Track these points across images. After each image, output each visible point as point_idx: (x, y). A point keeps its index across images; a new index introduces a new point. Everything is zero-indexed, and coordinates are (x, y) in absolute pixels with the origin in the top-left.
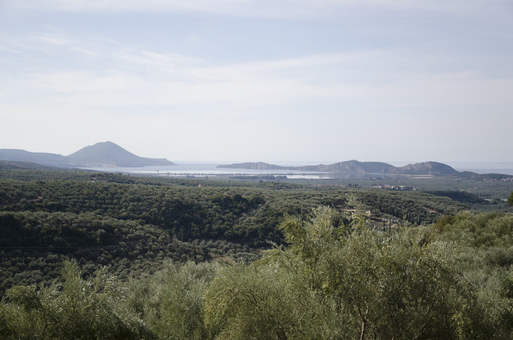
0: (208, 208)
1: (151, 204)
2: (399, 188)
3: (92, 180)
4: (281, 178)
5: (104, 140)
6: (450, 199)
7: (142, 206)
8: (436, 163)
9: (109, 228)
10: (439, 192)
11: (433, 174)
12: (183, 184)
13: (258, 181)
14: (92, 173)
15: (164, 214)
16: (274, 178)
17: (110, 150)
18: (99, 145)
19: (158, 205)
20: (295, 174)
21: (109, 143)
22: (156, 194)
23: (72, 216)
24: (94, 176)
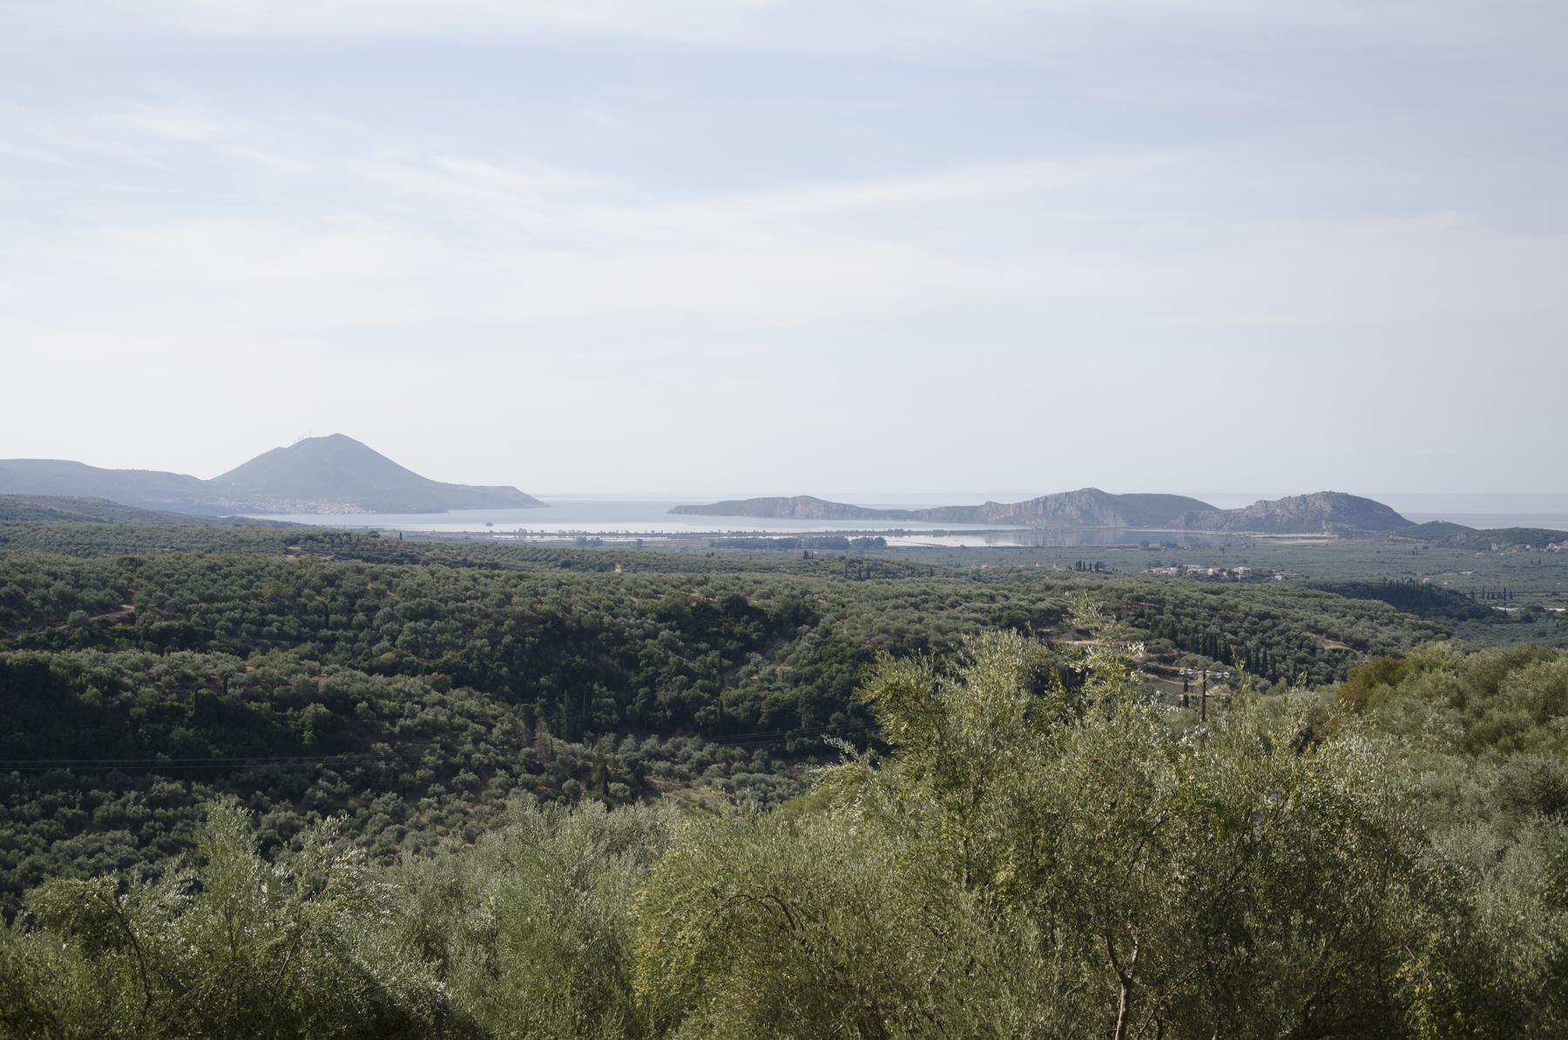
0: (643, 638)
1: (469, 626)
2: (1230, 573)
3: (287, 552)
4: (867, 544)
5: (323, 429)
6: (1387, 606)
7: (442, 631)
8: (1345, 496)
9: (340, 702)
10: (1354, 585)
11: (1336, 530)
12: (566, 565)
13: (797, 553)
14: (286, 533)
15: (508, 656)
16: (846, 545)
17: (342, 460)
18: (310, 447)
19: (491, 630)
20: (909, 533)
21: (338, 438)
22: (485, 595)
23: (227, 663)
24: (294, 542)
